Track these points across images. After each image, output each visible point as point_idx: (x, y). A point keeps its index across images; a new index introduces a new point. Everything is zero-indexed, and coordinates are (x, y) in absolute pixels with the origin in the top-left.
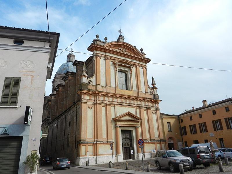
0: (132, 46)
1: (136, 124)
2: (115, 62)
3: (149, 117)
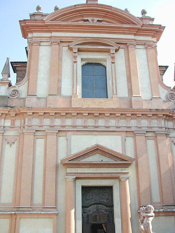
0: (111, 7)
1: (119, 170)
2: (72, 45)
3: (160, 154)
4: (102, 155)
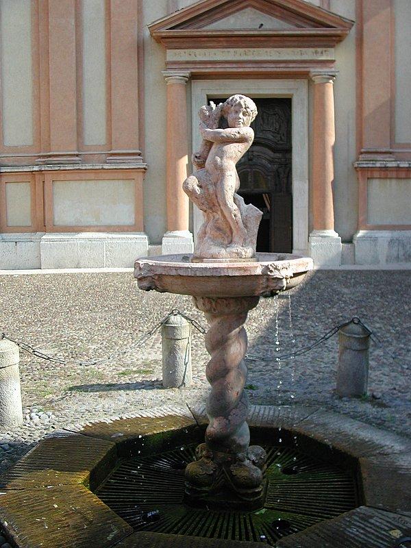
1: (308, 54)
4: (262, 10)
